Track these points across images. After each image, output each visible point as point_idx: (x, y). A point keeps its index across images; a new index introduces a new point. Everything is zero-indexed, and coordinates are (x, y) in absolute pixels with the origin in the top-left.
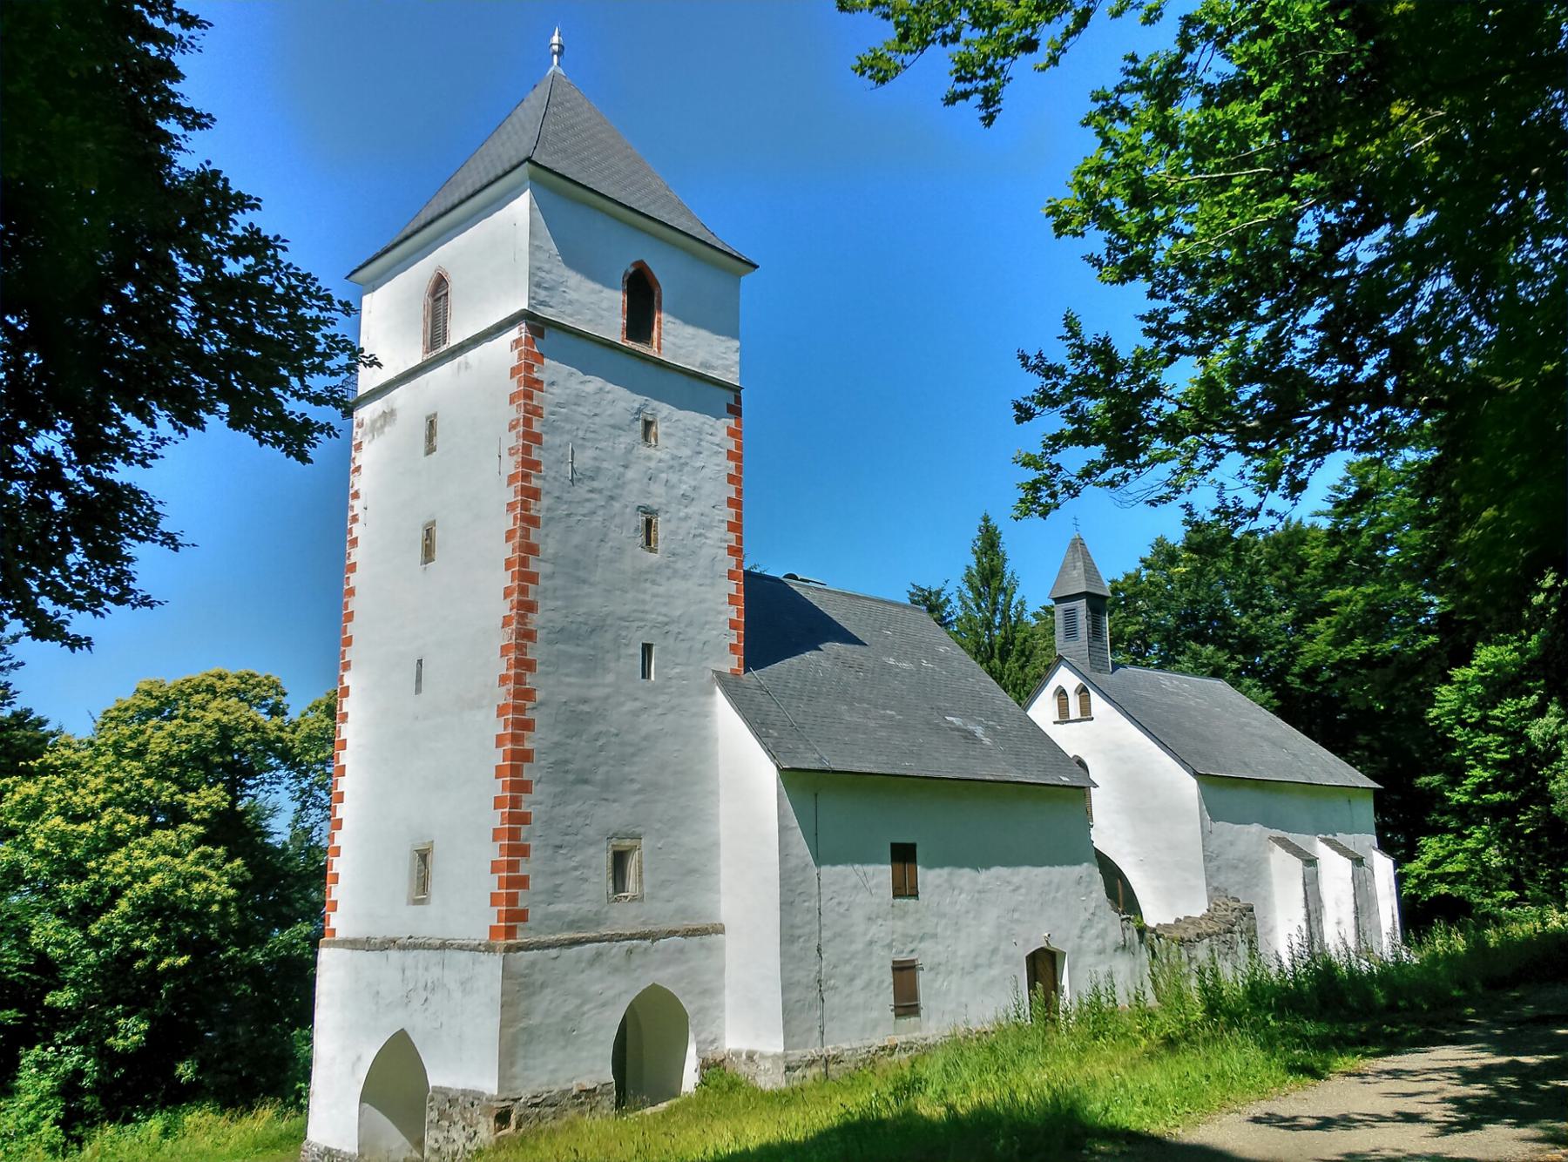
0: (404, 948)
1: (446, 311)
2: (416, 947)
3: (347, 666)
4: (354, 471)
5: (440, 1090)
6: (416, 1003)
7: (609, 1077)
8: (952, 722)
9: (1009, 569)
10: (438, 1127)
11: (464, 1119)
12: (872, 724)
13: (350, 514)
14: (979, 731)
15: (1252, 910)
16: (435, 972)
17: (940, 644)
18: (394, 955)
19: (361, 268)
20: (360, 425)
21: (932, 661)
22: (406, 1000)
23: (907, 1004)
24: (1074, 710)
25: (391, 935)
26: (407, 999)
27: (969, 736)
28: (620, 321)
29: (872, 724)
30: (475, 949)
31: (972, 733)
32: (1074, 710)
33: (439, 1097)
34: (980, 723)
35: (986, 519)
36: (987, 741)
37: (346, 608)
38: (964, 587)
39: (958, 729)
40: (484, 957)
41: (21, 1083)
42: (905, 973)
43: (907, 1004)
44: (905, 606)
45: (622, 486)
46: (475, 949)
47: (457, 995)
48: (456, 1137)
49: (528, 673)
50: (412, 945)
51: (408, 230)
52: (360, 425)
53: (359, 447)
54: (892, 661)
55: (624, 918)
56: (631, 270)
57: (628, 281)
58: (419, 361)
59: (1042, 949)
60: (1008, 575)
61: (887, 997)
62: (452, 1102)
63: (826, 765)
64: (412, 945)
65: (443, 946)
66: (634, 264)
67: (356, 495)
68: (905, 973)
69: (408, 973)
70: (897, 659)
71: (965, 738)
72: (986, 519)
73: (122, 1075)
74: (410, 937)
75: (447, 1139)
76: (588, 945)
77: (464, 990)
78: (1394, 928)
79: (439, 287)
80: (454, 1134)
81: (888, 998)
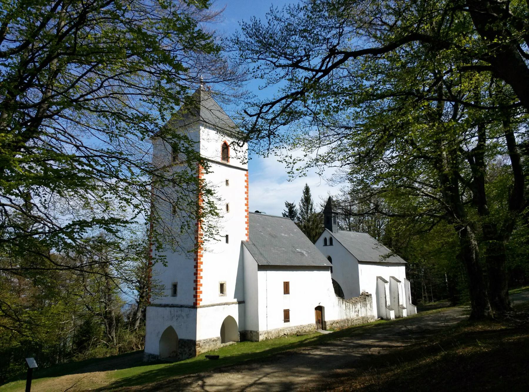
7: (219, 335)
9: (311, 198)
14: (305, 253)
16: (179, 313)
18: (168, 309)
23: (287, 318)
24: (328, 243)
27: (302, 254)
28: (220, 154)
32: (328, 243)
34: (304, 251)
36: (306, 255)
38: (301, 202)
43: (287, 318)
44: (281, 218)
45: (116, 137)
50: (172, 306)
54: (283, 235)
64: (172, 306)
73: (507, 82)
78: (448, 321)
80: (186, 349)
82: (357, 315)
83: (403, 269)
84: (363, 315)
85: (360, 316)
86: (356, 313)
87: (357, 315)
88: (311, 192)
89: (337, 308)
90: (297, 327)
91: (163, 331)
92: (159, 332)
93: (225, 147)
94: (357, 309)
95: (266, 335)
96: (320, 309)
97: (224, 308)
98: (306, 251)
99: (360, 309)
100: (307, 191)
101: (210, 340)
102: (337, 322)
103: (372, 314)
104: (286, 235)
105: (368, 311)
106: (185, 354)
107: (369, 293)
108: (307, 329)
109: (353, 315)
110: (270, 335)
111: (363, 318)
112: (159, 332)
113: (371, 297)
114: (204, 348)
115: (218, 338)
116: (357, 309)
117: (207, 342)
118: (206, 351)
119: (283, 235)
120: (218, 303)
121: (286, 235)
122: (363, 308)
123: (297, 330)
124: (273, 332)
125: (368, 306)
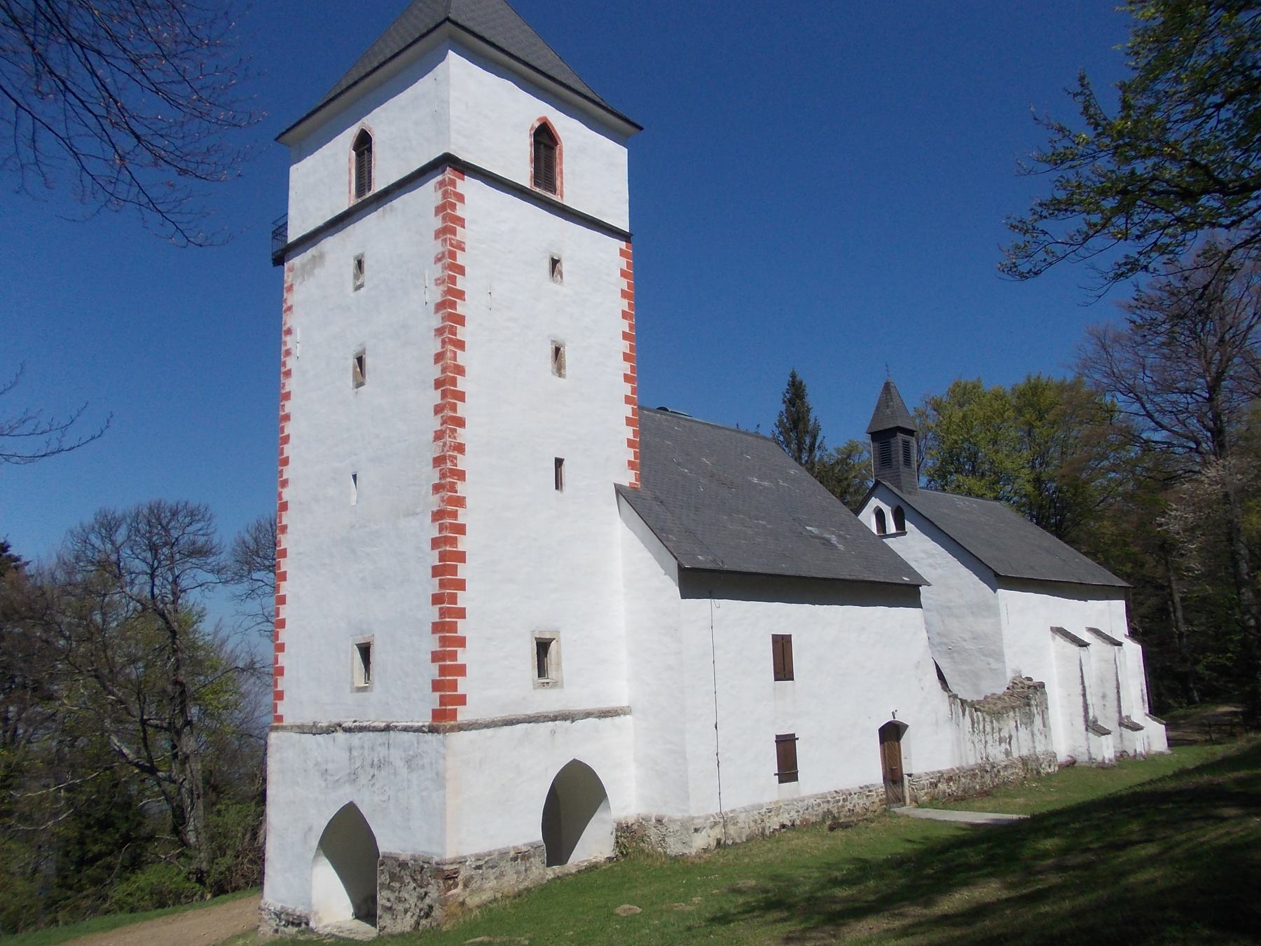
0: (348, 730)
1: (370, 162)
2: (361, 729)
3: (284, 483)
4: (286, 311)
5: (389, 857)
6: (363, 779)
7: (537, 835)
8: (811, 531)
10: (389, 888)
11: (415, 880)
12: (750, 532)
13: (284, 349)
14: (834, 539)
15: (1044, 687)
16: (383, 752)
17: (790, 468)
18: (340, 735)
19: (288, 130)
20: (291, 270)
21: (785, 480)
22: (353, 777)
23: (787, 769)
25: (335, 720)
26: (353, 777)
29: (750, 532)
30: (419, 730)
31: (828, 541)
33: (389, 862)
34: (833, 533)
35: (793, 376)
36: (841, 547)
37: (283, 432)
39: (816, 537)
40: (429, 736)
41: (1205, 756)
42: (786, 746)
43: (787, 769)
46: (419, 730)
47: (404, 771)
48: (407, 896)
49: (459, 482)
51: (332, 95)
52: (291, 270)
53: (290, 288)
54: (755, 480)
55: (549, 701)
56: (537, 125)
57: (534, 134)
58: (346, 208)
59: (889, 724)
60: (812, 421)
61: (772, 764)
62: (403, 865)
63: (719, 566)
65: (387, 729)
66: (539, 120)
67: (289, 332)
68: (786, 746)
69: (355, 753)
70: (760, 478)
71: (823, 544)
72: (793, 376)
74: (355, 721)
75: (399, 900)
76: (519, 726)
77: (409, 767)
79: (364, 144)
80: (404, 895)
81: (774, 767)
82: (1008, 753)
83: (1119, 606)
84: (1025, 752)
85: (1015, 754)
86: (1004, 746)
87: (1008, 753)
88: (813, 399)
89: (947, 734)
90: (824, 798)
91: (325, 823)
92: (310, 829)
93: (544, 139)
94: (1005, 734)
95: (717, 832)
96: (892, 733)
97: (553, 732)
98: (839, 536)
99: (1014, 733)
100: (796, 393)
101: (503, 854)
102: (950, 779)
103: (1050, 749)
104: (766, 484)
105: (1038, 737)
106: (406, 911)
107: (1036, 680)
108: (859, 803)
109: (997, 753)
110: (732, 830)
111: (1024, 761)
112: (310, 829)
113: (1044, 693)
114: (480, 890)
115: (536, 847)
116: (1005, 734)
117: (486, 863)
118: (485, 897)
119: (755, 480)
120: (531, 711)
121: (766, 484)
122: (1022, 730)
123: (825, 807)
124: (742, 817)
125: (1038, 720)
